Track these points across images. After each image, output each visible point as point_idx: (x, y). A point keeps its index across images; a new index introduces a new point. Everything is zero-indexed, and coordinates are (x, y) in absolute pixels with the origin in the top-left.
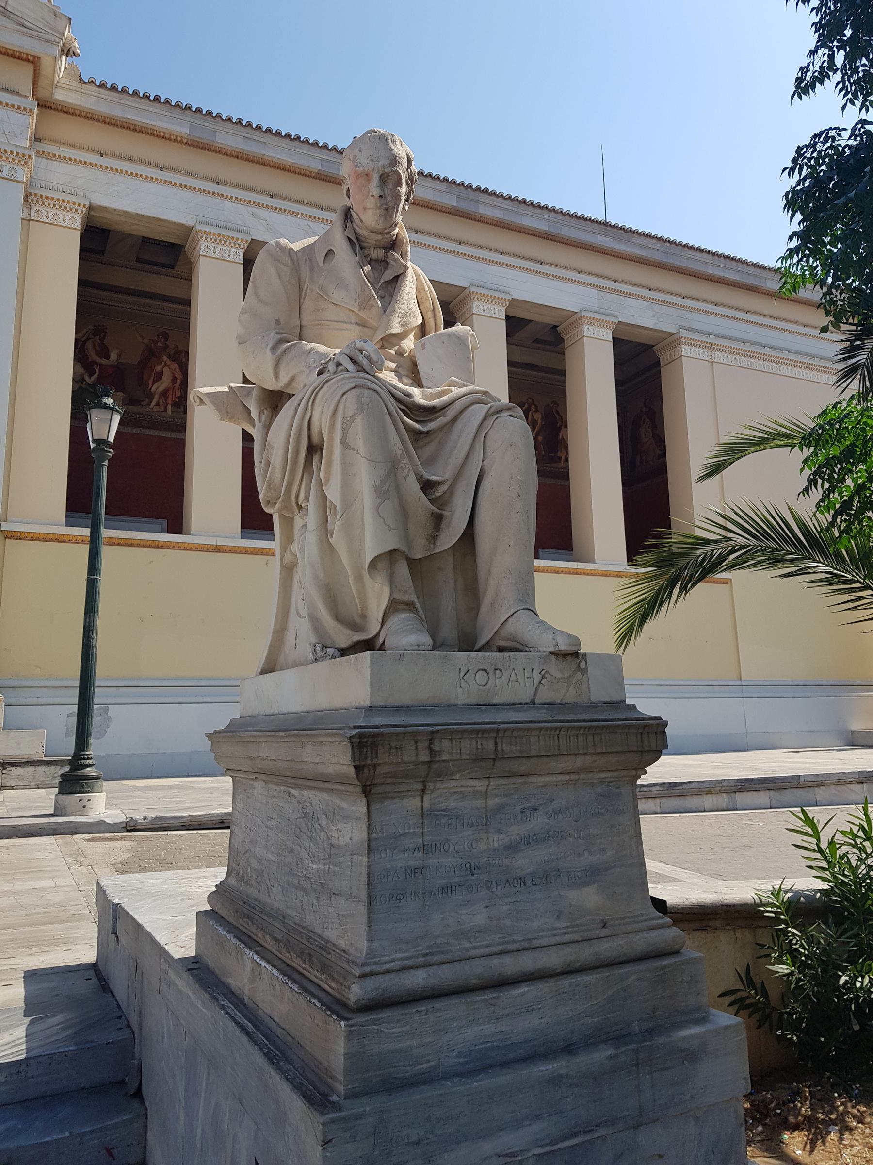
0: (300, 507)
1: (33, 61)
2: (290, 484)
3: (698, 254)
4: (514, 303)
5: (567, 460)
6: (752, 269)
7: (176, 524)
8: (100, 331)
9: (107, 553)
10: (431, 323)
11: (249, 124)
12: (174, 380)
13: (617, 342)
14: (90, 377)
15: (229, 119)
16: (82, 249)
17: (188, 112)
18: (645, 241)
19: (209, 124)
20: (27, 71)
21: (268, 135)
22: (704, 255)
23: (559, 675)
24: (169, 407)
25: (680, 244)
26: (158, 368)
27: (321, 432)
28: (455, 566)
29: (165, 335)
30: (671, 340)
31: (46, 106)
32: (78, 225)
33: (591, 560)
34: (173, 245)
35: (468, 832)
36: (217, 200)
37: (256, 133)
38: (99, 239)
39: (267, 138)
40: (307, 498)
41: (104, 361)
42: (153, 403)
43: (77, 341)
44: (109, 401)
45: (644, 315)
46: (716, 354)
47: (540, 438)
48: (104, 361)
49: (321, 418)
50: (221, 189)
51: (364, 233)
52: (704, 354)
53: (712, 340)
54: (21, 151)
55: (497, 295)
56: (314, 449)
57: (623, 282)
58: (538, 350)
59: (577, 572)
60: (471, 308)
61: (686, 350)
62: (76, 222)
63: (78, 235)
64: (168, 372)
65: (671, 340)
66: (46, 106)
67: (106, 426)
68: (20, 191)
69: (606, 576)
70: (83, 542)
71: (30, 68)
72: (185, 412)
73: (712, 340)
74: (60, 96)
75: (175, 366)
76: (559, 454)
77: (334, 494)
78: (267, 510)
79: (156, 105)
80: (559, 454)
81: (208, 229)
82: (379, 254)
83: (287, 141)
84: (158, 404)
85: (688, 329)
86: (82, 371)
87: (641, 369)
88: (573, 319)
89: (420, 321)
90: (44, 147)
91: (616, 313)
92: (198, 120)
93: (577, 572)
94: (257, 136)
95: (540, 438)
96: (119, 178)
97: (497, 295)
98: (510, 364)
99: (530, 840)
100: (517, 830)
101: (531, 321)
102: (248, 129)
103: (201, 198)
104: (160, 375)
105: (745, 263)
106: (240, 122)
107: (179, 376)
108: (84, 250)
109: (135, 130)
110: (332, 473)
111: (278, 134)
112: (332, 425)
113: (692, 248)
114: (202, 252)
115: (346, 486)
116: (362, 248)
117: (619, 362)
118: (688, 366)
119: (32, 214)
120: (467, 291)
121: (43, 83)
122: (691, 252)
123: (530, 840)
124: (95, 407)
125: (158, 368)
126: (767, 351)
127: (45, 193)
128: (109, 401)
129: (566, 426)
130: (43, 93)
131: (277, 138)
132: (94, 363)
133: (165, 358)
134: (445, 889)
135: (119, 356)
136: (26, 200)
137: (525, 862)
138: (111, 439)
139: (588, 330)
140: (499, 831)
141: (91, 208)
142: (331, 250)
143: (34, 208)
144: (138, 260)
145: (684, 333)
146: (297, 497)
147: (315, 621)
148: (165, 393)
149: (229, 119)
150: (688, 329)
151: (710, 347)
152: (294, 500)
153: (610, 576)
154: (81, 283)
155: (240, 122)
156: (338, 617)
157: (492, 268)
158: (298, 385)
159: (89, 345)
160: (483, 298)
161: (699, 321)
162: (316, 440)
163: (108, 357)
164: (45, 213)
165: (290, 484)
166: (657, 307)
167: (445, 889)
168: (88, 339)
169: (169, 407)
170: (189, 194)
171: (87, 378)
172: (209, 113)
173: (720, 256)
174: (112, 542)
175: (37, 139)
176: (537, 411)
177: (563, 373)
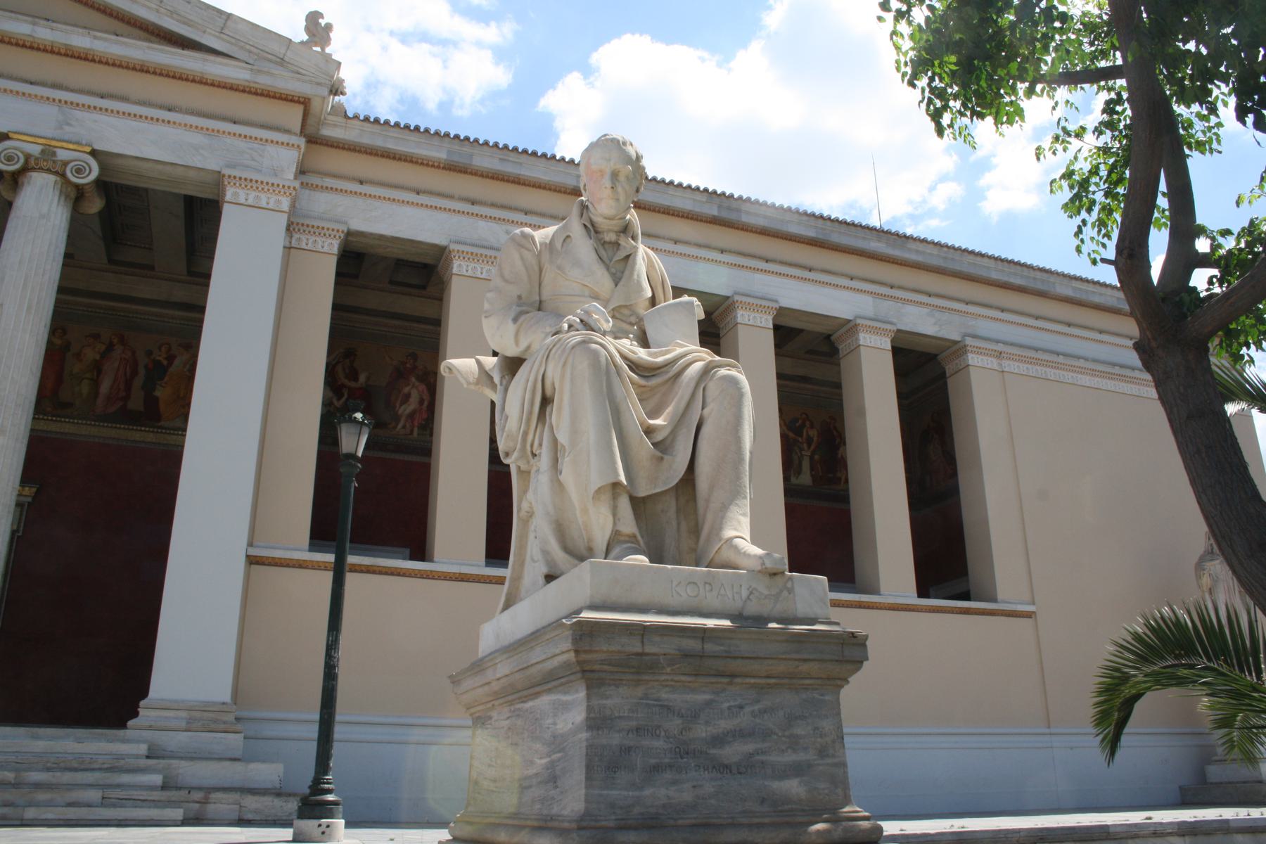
0: (534, 455)
1: (305, 102)
2: (526, 434)
3: (979, 259)
4: (782, 312)
5: (847, 481)
6: (1039, 275)
7: (420, 550)
8: (350, 354)
9: (351, 579)
10: (660, 295)
11: (506, 147)
12: (421, 402)
13: (897, 351)
14: (339, 399)
15: (486, 143)
16: (338, 274)
17: (447, 139)
18: (921, 247)
19: (467, 149)
20: (298, 111)
21: (525, 156)
22: (986, 260)
23: (766, 592)
24: (416, 430)
25: (959, 249)
26: (406, 390)
27: (553, 384)
28: (678, 511)
29: (414, 357)
30: (956, 349)
31: (314, 140)
32: (335, 250)
33: (875, 591)
34: (425, 266)
35: (678, 721)
36: (471, 220)
37: (512, 154)
38: (356, 261)
39: (524, 158)
40: (540, 445)
41: (353, 384)
42: (400, 426)
43: (328, 365)
44: (359, 416)
45: (923, 321)
46: (1005, 363)
47: (816, 457)
48: (353, 384)
49: (553, 373)
50: (476, 209)
51: (598, 220)
52: (992, 363)
53: (1000, 347)
54: (287, 184)
55: (764, 303)
56: (546, 401)
57: (900, 288)
58: (809, 360)
59: (860, 605)
60: (735, 317)
61: (973, 359)
62: (332, 247)
63: (334, 260)
64: (415, 393)
65: (956, 349)
66: (314, 140)
67: (355, 442)
68: (283, 220)
69: (894, 609)
70: (326, 569)
71: (301, 108)
72: (431, 435)
73: (1000, 347)
74: (326, 132)
75: (422, 387)
76: (839, 475)
77: (563, 438)
78: (506, 461)
79: (417, 134)
80: (839, 475)
81: (462, 248)
82: (610, 237)
83: (543, 160)
84: (404, 427)
85: (975, 336)
86: (330, 394)
87: (926, 377)
88: (849, 327)
89: (649, 294)
90: (306, 179)
91: (895, 320)
92: (456, 147)
93: (860, 605)
94: (513, 157)
95: (816, 457)
96: (377, 203)
97: (764, 303)
98: (780, 376)
99: (740, 734)
100: (724, 725)
101: (801, 331)
102: (505, 151)
103: (456, 218)
104: (408, 396)
105: (1030, 267)
106: (496, 145)
107: (426, 397)
108: (339, 274)
109: (394, 158)
110: (560, 417)
111: (534, 154)
112: (563, 376)
113: (972, 252)
114: (455, 270)
115: (575, 432)
116: (596, 232)
117: (902, 372)
118: (976, 378)
119: (294, 241)
120: (730, 301)
121: (311, 121)
122: (971, 257)
123: (740, 734)
124: (345, 421)
125: (406, 390)
126: (1061, 359)
127: (307, 222)
128: (359, 416)
129: (845, 444)
130: (310, 130)
131: (533, 159)
132: (343, 386)
133: (413, 379)
134: (657, 768)
135: (368, 378)
136: (288, 229)
137: (733, 752)
138: (360, 454)
139: (865, 338)
140: (707, 723)
141: (349, 233)
142: (568, 237)
143: (296, 236)
144: (391, 282)
145: (969, 341)
146: (532, 446)
147: (545, 553)
148: (411, 416)
149: (486, 143)
150: (975, 336)
151: (999, 355)
152: (529, 448)
153: (898, 609)
154: (336, 307)
155: (496, 145)
156: (566, 549)
157: (758, 276)
158: (535, 346)
159: (339, 368)
160: (749, 307)
161: (986, 327)
162: (548, 393)
163: (356, 379)
164: (306, 241)
165: (526, 434)
166: (937, 314)
167: (657, 768)
168: (338, 362)
169: (416, 430)
170: (444, 215)
171: (336, 402)
172: (467, 139)
173: (1002, 260)
174: (357, 569)
175: (302, 171)
176: (812, 427)
177: (838, 386)
